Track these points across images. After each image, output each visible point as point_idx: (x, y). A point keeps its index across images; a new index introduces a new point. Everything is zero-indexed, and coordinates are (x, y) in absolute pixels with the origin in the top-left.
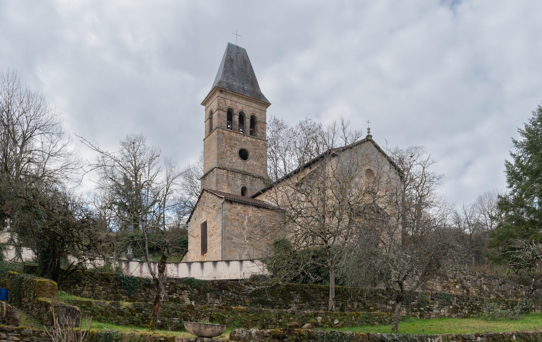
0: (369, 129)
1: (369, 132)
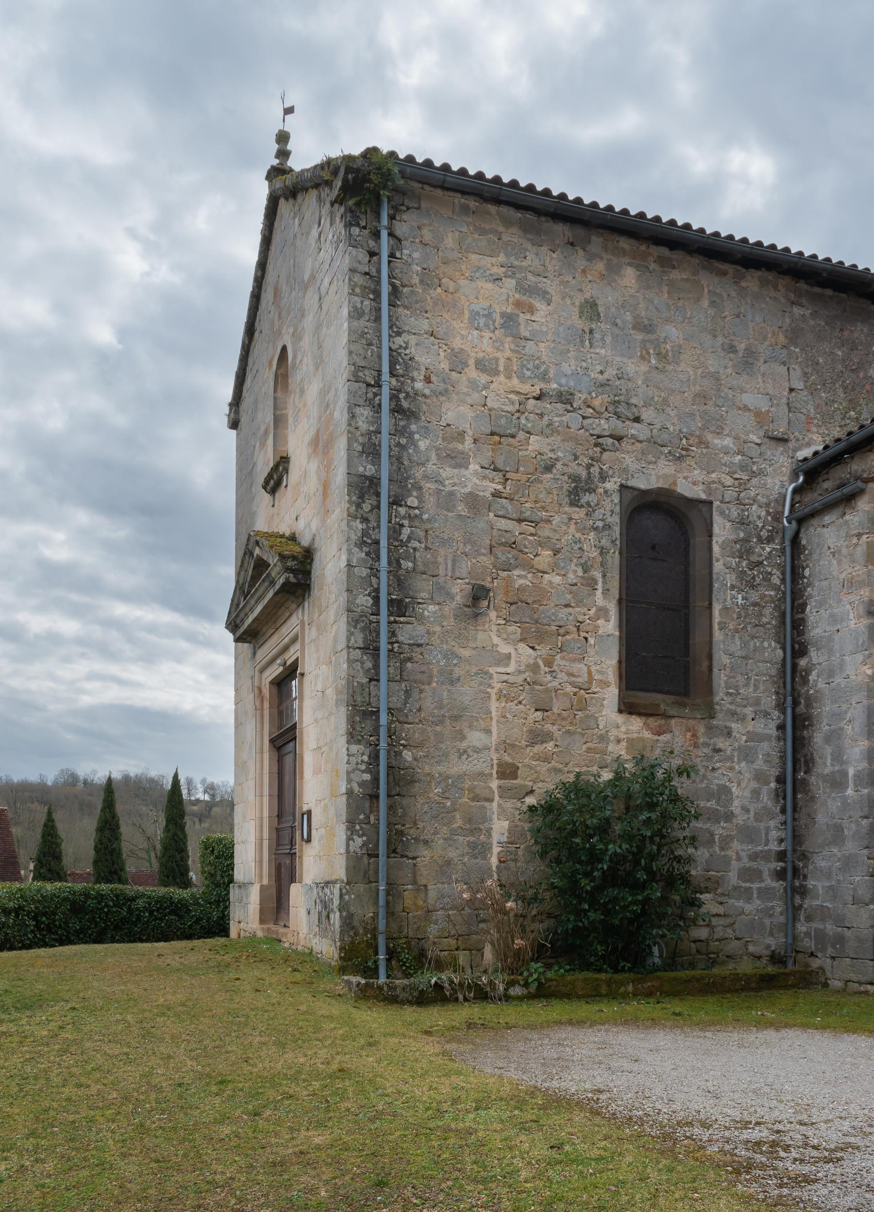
0: (283, 138)
1: (283, 154)
